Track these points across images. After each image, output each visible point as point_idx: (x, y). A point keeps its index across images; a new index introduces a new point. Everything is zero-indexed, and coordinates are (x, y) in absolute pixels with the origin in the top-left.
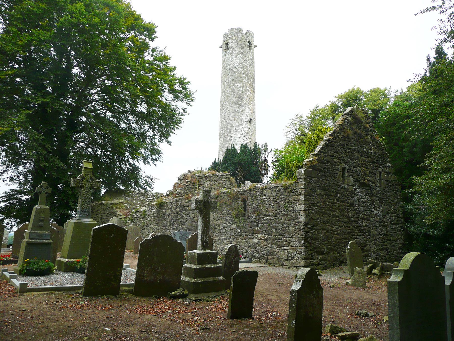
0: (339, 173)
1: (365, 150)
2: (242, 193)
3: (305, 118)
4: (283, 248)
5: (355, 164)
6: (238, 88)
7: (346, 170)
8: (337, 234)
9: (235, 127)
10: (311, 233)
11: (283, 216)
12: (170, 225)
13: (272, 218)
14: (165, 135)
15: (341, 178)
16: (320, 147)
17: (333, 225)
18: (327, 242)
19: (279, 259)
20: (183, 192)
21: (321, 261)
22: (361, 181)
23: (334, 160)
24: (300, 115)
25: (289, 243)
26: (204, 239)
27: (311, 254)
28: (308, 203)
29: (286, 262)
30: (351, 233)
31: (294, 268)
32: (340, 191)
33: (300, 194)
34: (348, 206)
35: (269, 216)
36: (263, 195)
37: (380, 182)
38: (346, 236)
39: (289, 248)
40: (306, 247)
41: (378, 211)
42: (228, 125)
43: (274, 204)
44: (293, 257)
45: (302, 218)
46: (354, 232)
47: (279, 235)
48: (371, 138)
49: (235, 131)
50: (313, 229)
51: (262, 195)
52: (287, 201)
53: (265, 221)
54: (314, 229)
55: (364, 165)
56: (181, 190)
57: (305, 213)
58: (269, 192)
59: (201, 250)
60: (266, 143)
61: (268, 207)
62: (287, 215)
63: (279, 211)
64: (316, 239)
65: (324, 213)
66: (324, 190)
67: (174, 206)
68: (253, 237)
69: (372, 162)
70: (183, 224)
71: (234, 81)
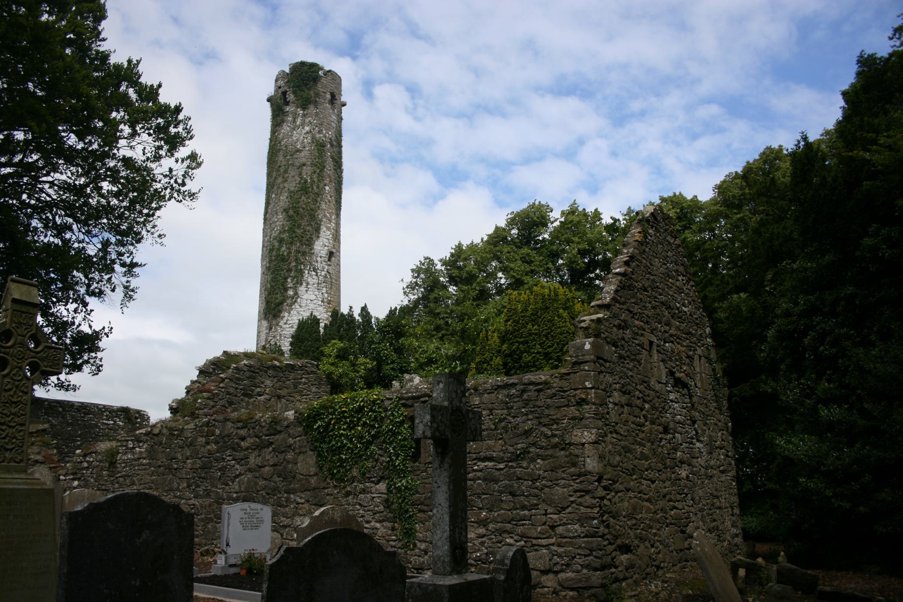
2: (409, 402)
4: (534, 541)
7: (655, 347)
10: (610, 500)
12: (189, 486)
13: (502, 466)
18: (634, 521)
20: (212, 403)
22: (677, 375)
23: (637, 322)
32: (648, 396)
35: (490, 459)
39: (553, 540)
45: (592, 464)
47: (524, 508)
50: (611, 491)
53: (479, 474)
65: (627, 450)
66: (624, 393)
67: (200, 439)
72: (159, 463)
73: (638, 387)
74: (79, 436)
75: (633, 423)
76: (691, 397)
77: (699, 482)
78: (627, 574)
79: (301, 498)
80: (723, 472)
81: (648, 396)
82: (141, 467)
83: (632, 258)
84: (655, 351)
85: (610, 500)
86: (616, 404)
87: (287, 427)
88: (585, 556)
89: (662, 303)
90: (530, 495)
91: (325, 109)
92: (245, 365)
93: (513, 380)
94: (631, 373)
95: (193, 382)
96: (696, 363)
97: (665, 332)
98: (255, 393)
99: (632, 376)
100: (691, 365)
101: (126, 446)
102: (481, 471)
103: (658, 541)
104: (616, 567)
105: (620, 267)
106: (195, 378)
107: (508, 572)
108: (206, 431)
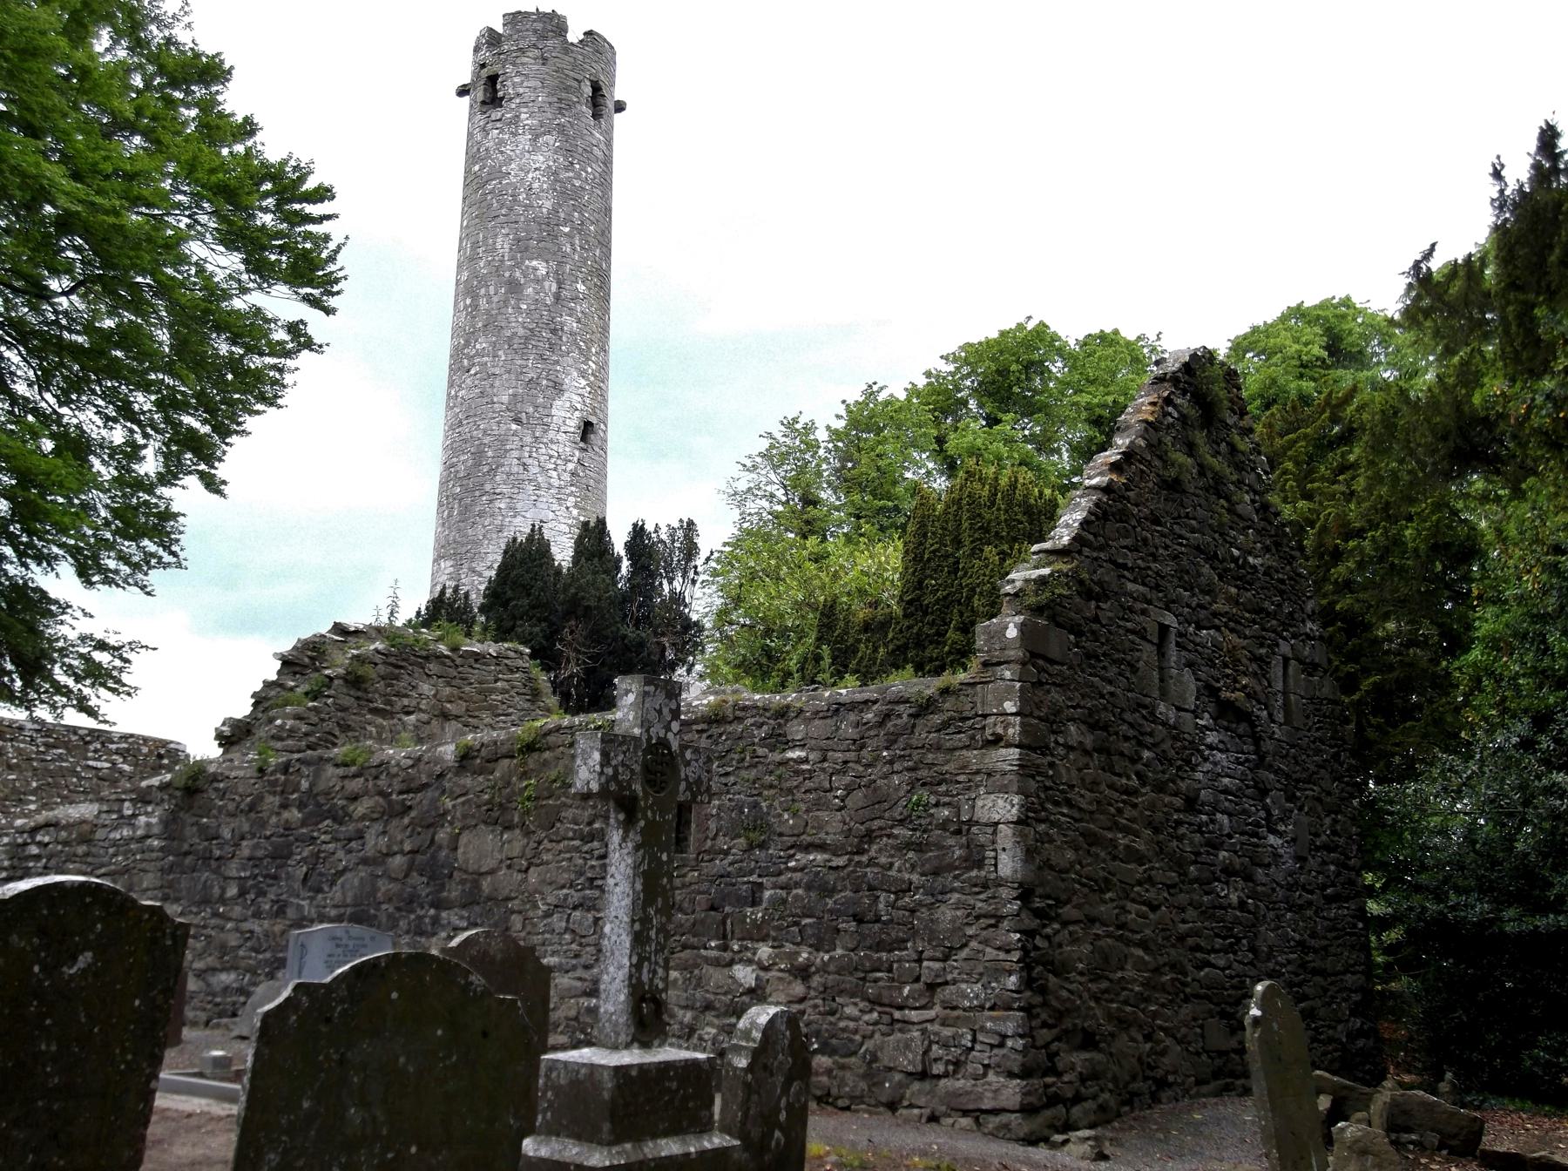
0: (1148, 647)
1: (1236, 552)
3: (822, 435)
4: (897, 1015)
5: (1203, 614)
6: (538, 281)
7: (1173, 637)
8: (1143, 944)
9: (515, 454)
10: (1048, 937)
11: (898, 848)
12: (242, 893)
13: (841, 861)
14: (196, 453)
15: (1155, 674)
16: (1079, 516)
17: (1127, 897)
18: (1104, 985)
19: (874, 1071)
20: (304, 728)
21: (1083, 1079)
22: (1225, 694)
23: (1130, 586)
24: (802, 420)
25: (931, 987)
26: (645, 977)
27: (1046, 1046)
28: (1032, 785)
29: (916, 1086)
30: (1190, 941)
31: (965, 1122)
32: (1151, 734)
33: (997, 741)
34: (1177, 811)
35: (822, 847)
36: (789, 744)
37: (1286, 706)
38: (1173, 951)
39: (931, 1014)
40: (1028, 1009)
41: (1280, 834)
42: (486, 440)
43: (849, 790)
44: (957, 1064)
45: (1008, 864)
46: (1197, 934)
47: (879, 946)
48: (1253, 501)
49: (515, 469)
50: (1052, 919)
51: (779, 740)
52: (923, 773)
53: (798, 876)
54: (1057, 918)
55: (1233, 623)
56: (298, 717)
57: (1023, 836)
58: (819, 727)
59: (628, 1046)
60: (691, 523)
61: (819, 805)
62: (919, 848)
63: (876, 824)
64: (1060, 969)
65: (1092, 839)
66: (1093, 727)
67: (269, 799)
68: (727, 955)
69: (1259, 610)
70: (319, 890)
71: (521, 247)
72: (186, 847)
73: (1127, 716)
74: (34, 792)
75: (1111, 786)
76: (1257, 740)
77: (1271, 914)
78: (1083, 1090)
79: (462, 918)
80: (1330, 900)
81: (1151, 734)
82: (147, 856)
83: (1129, 455)
84: (1173, 645)
85: (1048, 937)
86: (1070, 748)
87: (441, 776)
88: (992, 1046)
89: (1197, 548)
90: (891, 921)
91: (578, 116)
92: (377, 651)
93: (871, 692)
94: (1110, 688)
95: (268, 685)
96: (1277, 671)
97: (1200, 606)
98: (398, 707)
99: (1112, 694)
100: (1263, 674)
101: (120, 811)
102: (802, 870)
103: (1161, 1028)
104: (1059, 1074)
105: (1101, 474)
106: (274, 677)
107: (757, 1055)
108: (276, 780)
